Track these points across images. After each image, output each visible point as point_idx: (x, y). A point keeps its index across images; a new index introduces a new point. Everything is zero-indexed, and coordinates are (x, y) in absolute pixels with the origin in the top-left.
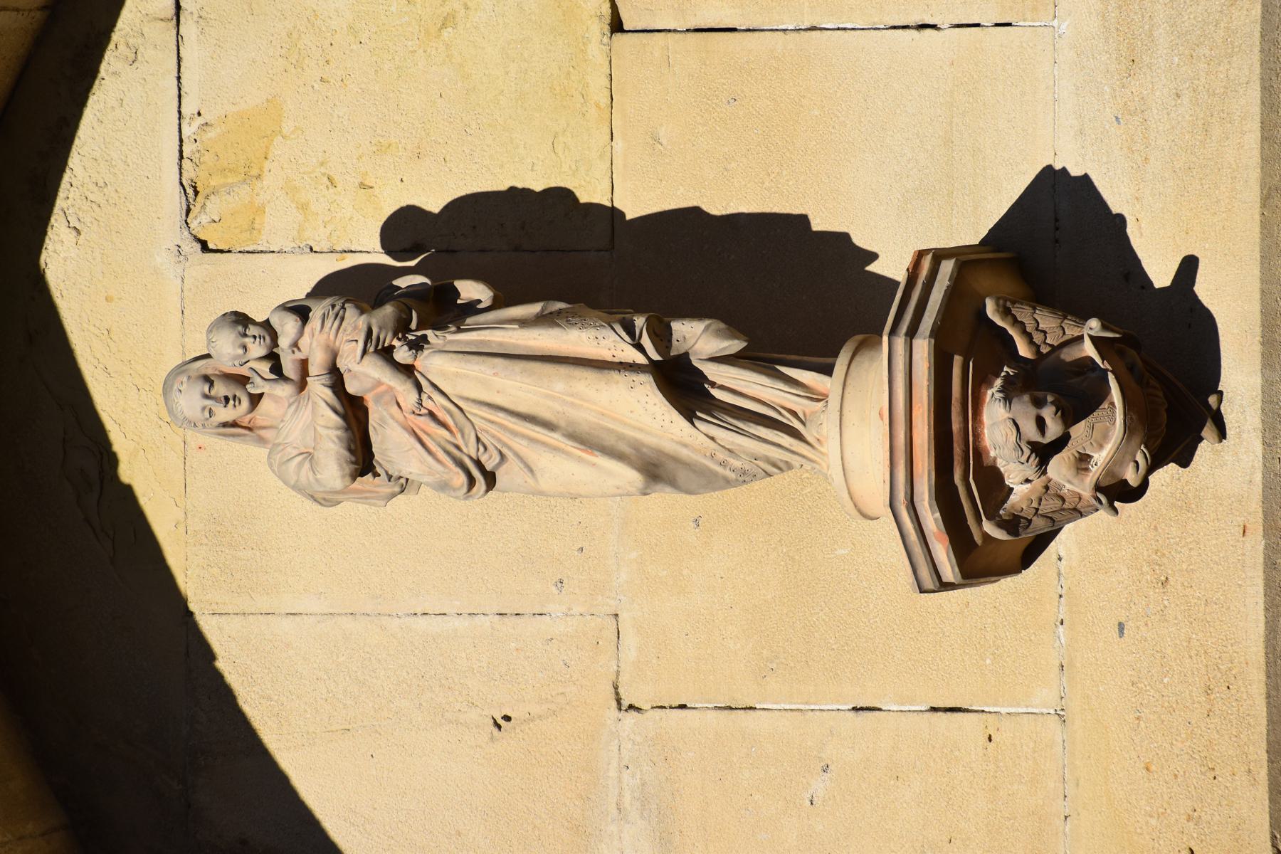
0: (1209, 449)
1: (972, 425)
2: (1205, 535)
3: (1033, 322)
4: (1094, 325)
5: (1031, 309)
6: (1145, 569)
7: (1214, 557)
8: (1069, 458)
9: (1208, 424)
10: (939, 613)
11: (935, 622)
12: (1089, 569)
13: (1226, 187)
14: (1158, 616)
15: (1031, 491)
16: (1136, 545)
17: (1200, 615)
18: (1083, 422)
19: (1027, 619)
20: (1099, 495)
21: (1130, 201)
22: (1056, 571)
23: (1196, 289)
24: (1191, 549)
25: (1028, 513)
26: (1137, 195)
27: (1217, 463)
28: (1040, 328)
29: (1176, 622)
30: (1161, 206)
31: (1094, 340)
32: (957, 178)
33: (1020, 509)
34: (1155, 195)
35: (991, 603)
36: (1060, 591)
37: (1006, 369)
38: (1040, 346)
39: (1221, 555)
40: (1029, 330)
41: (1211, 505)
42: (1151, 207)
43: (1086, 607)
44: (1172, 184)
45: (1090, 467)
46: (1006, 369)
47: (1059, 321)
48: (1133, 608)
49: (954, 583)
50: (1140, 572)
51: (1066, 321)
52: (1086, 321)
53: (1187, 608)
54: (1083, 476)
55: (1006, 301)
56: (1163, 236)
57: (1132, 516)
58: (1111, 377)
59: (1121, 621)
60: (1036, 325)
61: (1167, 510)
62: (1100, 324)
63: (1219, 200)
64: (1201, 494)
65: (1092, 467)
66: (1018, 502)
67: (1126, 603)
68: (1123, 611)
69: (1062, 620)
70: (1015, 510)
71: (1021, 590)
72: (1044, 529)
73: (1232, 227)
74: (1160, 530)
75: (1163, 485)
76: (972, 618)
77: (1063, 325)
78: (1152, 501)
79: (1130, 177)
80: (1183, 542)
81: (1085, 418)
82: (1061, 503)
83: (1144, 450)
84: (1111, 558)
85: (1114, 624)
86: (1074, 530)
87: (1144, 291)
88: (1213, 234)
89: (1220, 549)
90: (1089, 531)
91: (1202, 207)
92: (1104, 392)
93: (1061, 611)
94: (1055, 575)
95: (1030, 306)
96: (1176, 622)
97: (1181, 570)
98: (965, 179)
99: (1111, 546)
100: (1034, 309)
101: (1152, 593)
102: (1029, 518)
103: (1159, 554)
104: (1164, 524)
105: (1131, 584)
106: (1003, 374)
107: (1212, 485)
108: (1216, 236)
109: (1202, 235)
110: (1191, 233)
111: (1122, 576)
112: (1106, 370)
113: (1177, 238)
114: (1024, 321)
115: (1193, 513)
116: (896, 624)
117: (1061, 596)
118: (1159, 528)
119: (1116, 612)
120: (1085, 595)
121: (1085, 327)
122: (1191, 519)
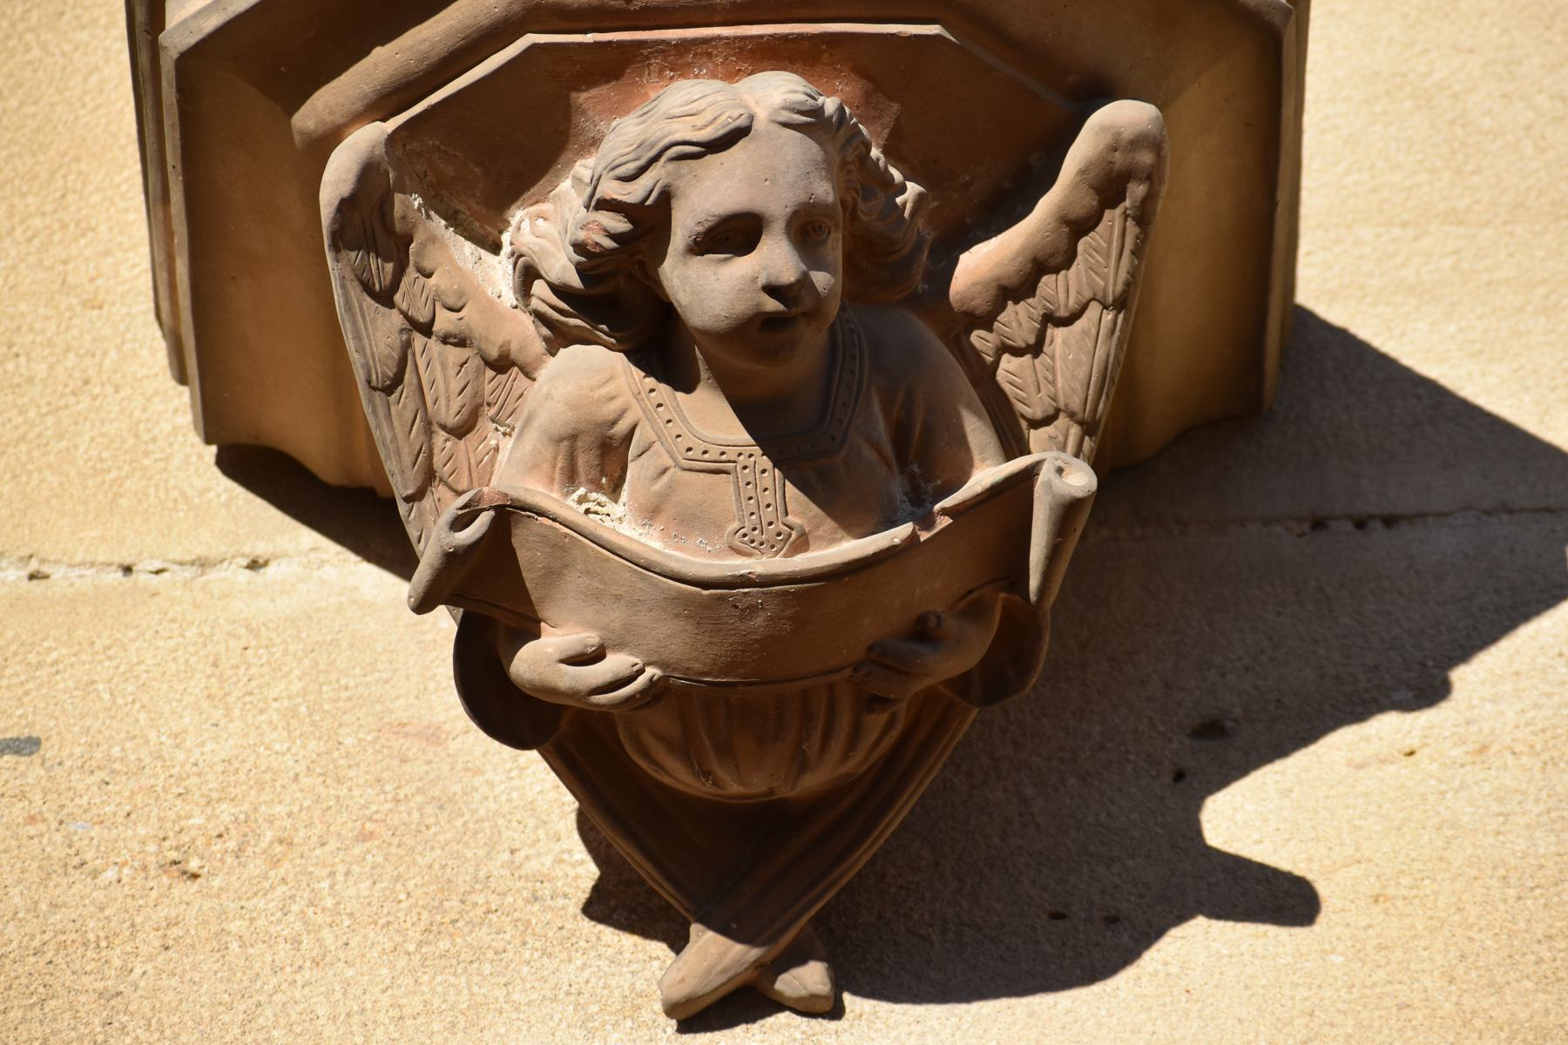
0: (640, 986)
1: (719, 38)
2: (347, 983)
3: (1072, 301)
4: (1080, 480)
5: (1119, 288)
6: (225, 812)
7: (269, 1013)
8: (612, 398)
9: (738, 948)
10: (64, 226)
11: (31, 216)
12: (222, 648)
13: (1547, 1012)
14: (62, 852)
15: (490, 307)
16: (305, 781)
17: (68, 978)
18: (745, 437)
19: (47, 474)
20: (484, 520)
21: (1474, 728)
22: (214, 554)
23: (1200, 922)
24: (296, 941)
25: (413, 294)
26: (1493, 749)
27: (594, 1008)
28: (1050, 331)
29: (44, 907)
30: (1465, 819)
31: (1019, 488)
32: (1511, 234)
33: (427, 264)
34: (1500, 800)
35: (99, 372)
36: (145, 565)
37: (913, 189)
38: (990, 329)
39: (275, 1033)
40: (1047, 283)
41: (451, 999)
42: (1457, 791)
43: (93, 643)
44: (1542, 851)
45: (582, 491)
46: (913, 189)
47: (1075, 403)
48: (93, 779)
49: (162, 28)
50: (215, 795)
51: (1075, 431)
52: (1094, 467)
53: (91, 937)
54: (546, 466)
55: (1149, 178)
56: (1360, 828)
57: (407, 768)
58: (899, 534)
59: (44, 745)
60: (1062, 313)
61: (430, 867)
62: (1080, 494)
63: (1499, 991)
64: (487, 968)
65: (581, 500)
66: (452, 261)
67: (109, 758)
68: (78, 751)
69: (46, 577)
70: (423, 246)
71: (146, 454)
72: (360, 350)
73: (1410, 1033)
74: (358, 849)
75: (512, 852)
76: (48, 318)
77: (1062, 421)
78: (459, 823)
79: (1555, 727)
80: (319, 919)
81: (760, 440)
82: (452, 420)
83: (641, 680)
84: (261, 712)
85: (34, 723)
86: (353, 602)
87: (1167, 779)
88: (1381, 974)
89: (298, 1029)
90: (352, 646)
91: (1471, 939)
92: (853, 521)
93: (77, 572)
94: (198, 551)
95: (1128, 284)
96: (44, 907)
97: (223, 915)
98: (1511, 255)
99: (303, 709)
100: (1120, 304)
101: (142, 832)
102: (398, 298)
103: (278, 849)
104: (380, 859)
105: (174, 771)
106: (897, 175)
107: (515, 997)
108: (1374, 984)
109: (1374, 942)
110: (1377, 909)
111: (202, 744)
112: (926, 521)
113: (1355, 870)
114: (1078, 266)
115: (420, 944)
116: (22, 105)
117: (128, 570)
118: (368, 844)
119: (76, 729)
120: (133, 640)
121: (1067, 456)
122: (398, 939)
